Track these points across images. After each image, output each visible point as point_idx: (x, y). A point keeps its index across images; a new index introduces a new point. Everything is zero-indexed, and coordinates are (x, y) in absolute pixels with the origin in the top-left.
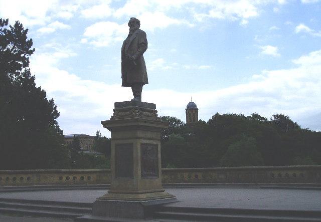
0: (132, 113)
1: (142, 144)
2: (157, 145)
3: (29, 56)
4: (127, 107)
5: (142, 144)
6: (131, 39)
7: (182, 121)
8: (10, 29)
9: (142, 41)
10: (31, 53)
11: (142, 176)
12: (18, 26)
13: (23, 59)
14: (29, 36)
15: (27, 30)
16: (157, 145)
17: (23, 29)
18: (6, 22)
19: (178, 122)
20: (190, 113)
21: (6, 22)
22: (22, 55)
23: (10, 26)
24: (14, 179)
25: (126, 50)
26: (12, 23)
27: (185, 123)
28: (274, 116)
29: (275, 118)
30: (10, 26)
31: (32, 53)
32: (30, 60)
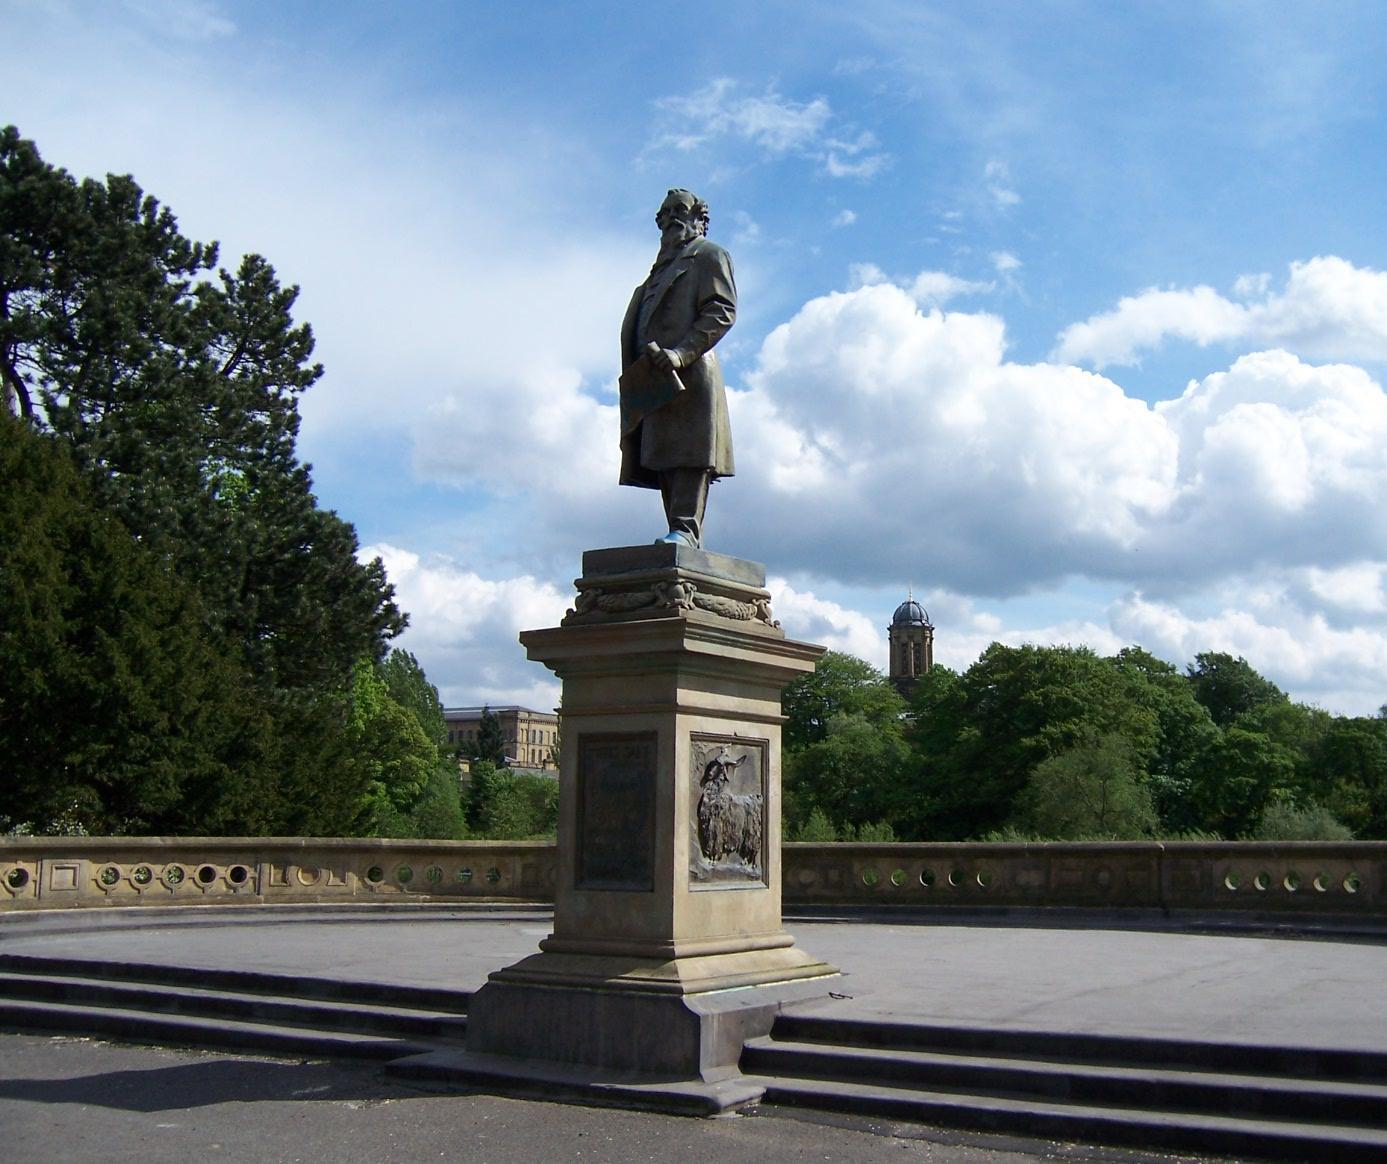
0: (655, 599)
1: (696, 737)
2: (763, 745)
3: (297, 394)
4: (637, 574)
5: (696, 737)
6: (667, 281)
7: (874, 666)
8: (221, 287)
9: (941, 1122)
10: (306, 380)
11: (694, 877)
12: (256, 271)
13: (274, 405)
14: (299, 316)
15: (294, 292)
16: (763, 745)
17: (274, 288)
18: (212, 255)
19: (859, 670)
20: (904, 639)
21: (212, 255)
22: (273, 389)
23: (224, 276)
24: (207, 875)
25: (643, 324)
26: (231, 262)
27: (886, 673)
28: (1200, 658)
29: (1203, 666)
30: (224, 276)
31: (310, 383)
32: (301, 410)
